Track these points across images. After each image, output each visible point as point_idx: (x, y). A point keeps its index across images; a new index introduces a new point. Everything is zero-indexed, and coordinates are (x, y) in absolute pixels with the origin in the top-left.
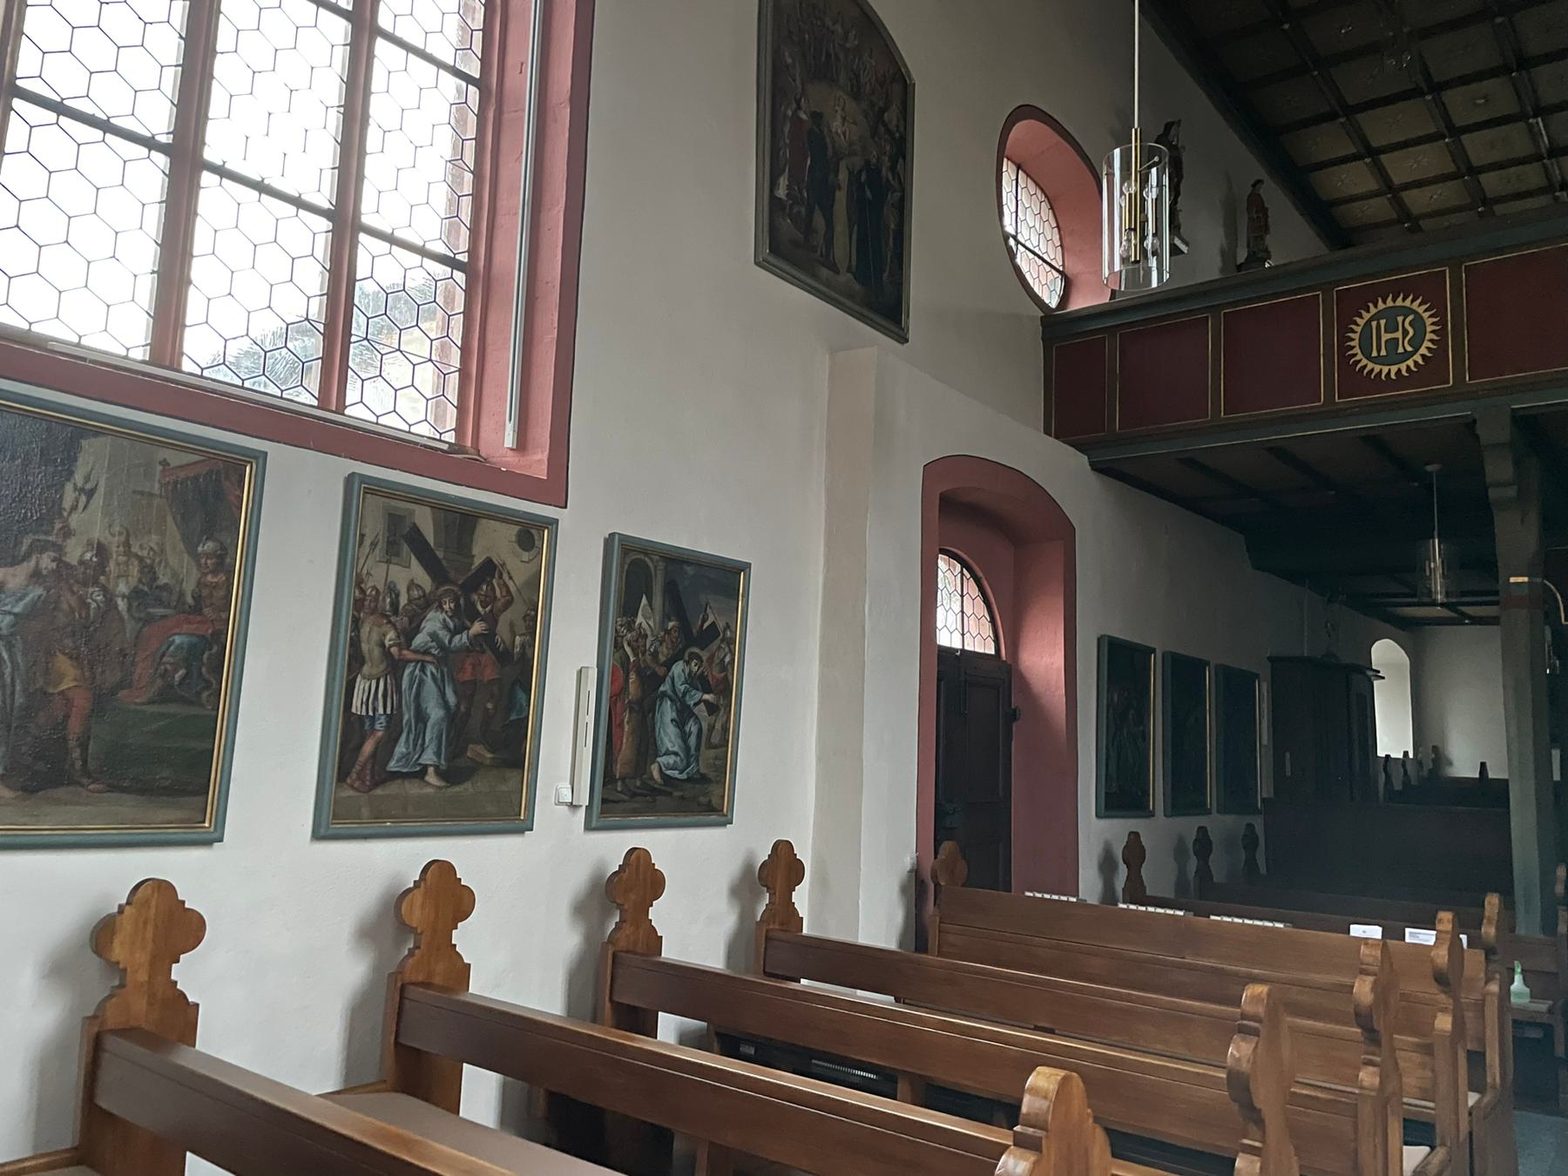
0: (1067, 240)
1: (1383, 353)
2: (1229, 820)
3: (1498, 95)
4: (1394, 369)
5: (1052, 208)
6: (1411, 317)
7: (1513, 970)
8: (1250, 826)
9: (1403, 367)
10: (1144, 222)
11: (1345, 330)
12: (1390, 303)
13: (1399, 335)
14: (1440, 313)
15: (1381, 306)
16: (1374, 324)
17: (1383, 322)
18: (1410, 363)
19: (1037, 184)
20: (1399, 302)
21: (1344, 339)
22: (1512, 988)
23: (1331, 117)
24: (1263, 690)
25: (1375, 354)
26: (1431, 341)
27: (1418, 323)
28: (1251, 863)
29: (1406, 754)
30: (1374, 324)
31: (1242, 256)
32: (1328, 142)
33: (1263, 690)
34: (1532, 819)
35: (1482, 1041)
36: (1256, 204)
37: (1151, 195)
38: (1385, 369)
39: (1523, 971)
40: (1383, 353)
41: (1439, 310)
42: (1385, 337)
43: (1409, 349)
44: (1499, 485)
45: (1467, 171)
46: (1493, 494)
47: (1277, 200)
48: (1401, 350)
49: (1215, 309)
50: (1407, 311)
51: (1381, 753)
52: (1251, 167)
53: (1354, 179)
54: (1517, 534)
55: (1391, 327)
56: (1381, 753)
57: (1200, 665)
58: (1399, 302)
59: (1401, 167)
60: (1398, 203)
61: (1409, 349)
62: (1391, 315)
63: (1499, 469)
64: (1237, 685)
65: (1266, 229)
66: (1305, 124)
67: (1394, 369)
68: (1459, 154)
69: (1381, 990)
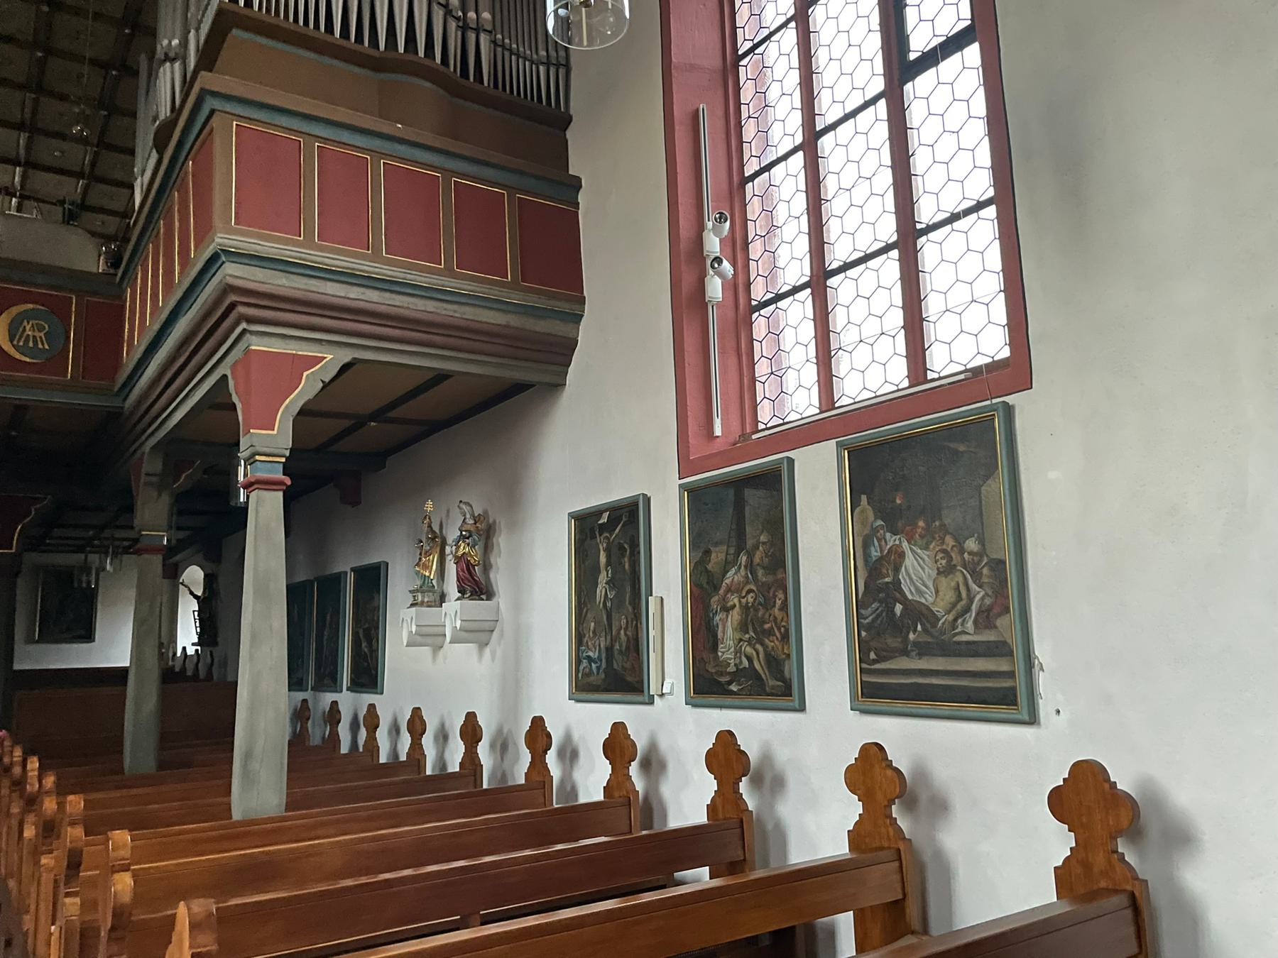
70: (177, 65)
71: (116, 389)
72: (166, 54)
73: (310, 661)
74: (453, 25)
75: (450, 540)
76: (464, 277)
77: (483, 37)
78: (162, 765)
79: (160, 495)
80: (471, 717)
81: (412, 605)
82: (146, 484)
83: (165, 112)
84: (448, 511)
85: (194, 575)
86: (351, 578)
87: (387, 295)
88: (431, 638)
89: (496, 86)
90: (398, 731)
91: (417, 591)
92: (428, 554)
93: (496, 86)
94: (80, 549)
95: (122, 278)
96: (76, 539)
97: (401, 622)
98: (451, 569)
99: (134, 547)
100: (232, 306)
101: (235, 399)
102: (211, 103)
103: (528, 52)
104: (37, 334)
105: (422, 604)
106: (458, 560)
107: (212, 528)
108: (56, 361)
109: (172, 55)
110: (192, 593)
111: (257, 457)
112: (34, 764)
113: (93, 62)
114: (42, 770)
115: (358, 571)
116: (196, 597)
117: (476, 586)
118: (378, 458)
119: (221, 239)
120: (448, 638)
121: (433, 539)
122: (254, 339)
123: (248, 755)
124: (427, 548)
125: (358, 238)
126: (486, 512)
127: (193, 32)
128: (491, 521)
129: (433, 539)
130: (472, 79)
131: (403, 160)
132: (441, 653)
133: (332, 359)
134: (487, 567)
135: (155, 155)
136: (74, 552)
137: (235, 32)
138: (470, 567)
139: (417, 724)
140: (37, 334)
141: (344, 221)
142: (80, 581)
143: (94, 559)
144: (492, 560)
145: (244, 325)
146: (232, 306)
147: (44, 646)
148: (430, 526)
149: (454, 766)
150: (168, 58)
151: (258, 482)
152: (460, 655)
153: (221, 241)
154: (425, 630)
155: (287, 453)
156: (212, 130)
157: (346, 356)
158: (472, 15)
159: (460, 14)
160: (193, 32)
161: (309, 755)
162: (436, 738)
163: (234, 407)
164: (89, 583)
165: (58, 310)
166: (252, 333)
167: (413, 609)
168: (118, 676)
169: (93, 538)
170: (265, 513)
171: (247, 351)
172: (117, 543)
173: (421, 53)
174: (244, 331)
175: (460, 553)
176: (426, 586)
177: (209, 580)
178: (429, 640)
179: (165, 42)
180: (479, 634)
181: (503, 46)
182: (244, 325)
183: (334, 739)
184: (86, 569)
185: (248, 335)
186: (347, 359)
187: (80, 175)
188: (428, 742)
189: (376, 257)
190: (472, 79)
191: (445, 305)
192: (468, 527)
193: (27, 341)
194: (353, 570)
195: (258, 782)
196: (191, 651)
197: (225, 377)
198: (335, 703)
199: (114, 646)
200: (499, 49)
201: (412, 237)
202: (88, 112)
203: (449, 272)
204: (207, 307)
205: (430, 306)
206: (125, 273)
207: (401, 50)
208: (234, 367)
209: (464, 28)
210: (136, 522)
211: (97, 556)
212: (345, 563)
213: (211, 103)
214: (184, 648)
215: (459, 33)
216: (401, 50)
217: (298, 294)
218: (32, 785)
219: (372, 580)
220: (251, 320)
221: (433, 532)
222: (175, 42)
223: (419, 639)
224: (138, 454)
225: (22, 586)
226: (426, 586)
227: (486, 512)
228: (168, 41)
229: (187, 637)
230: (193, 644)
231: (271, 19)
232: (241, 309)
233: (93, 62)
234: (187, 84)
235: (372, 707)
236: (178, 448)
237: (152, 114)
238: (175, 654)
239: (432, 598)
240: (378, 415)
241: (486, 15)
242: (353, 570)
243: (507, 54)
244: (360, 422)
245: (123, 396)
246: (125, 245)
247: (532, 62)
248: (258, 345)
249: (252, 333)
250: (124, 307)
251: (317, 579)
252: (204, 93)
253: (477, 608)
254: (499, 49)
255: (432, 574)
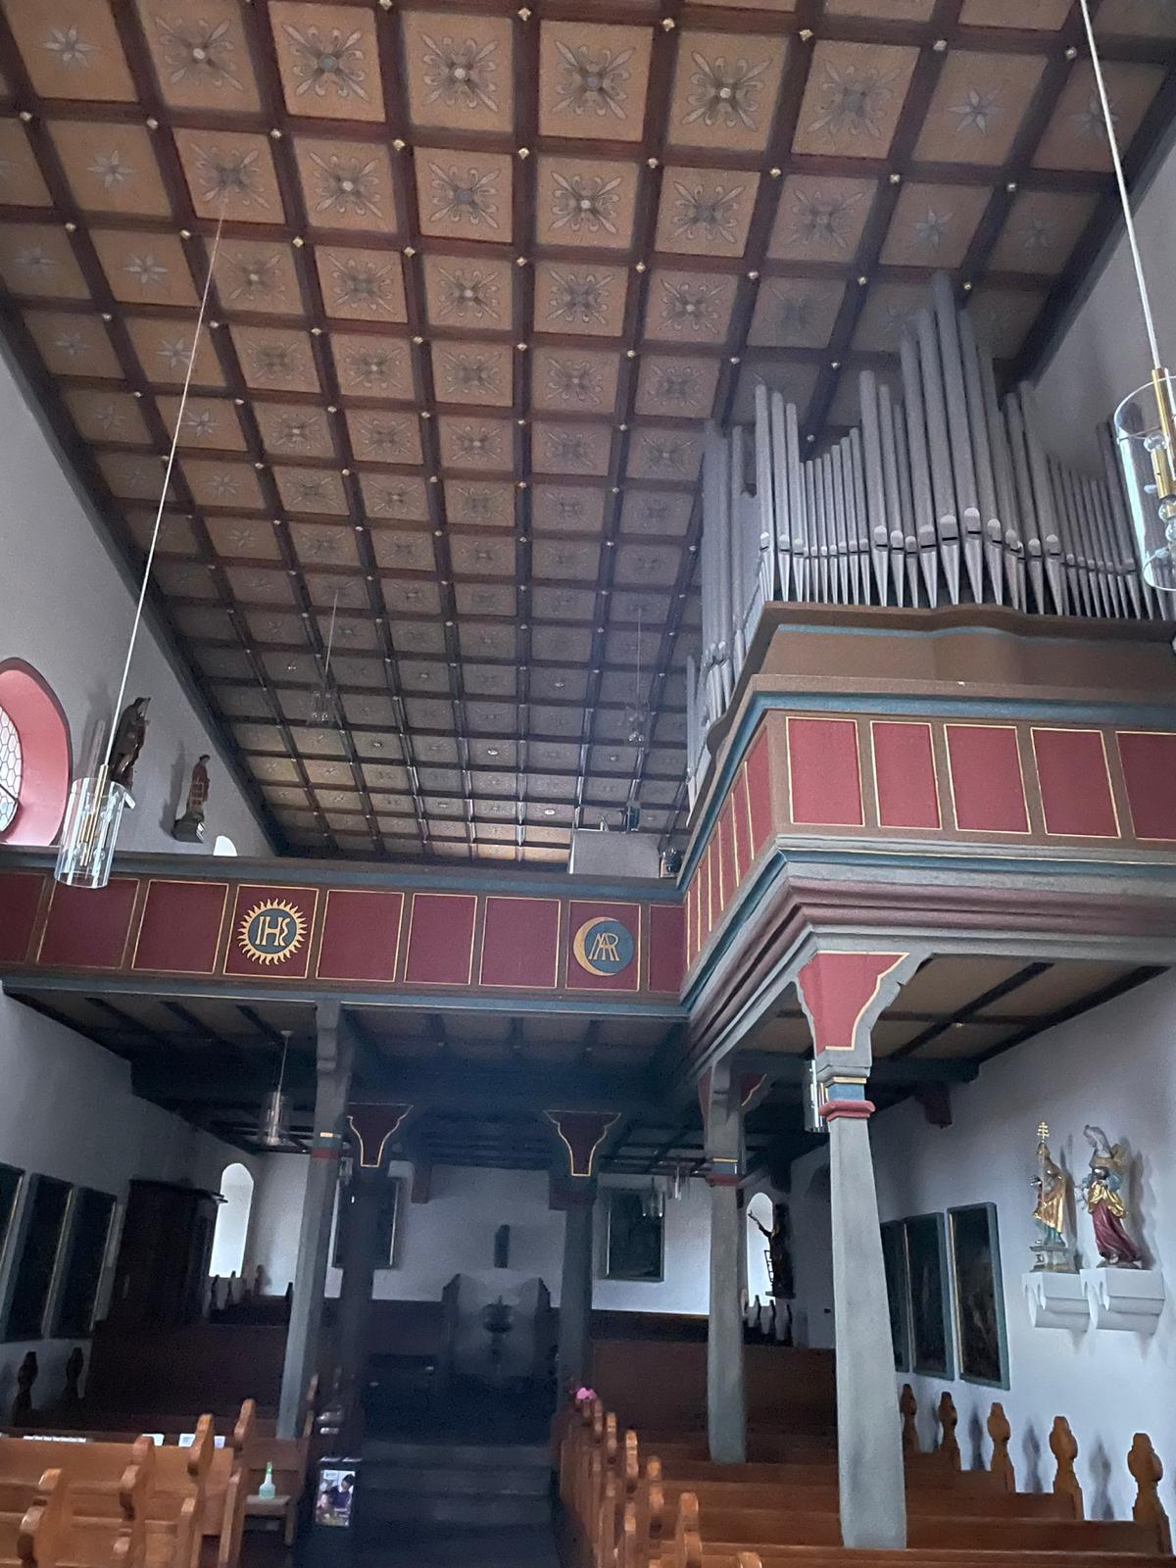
0: (28, 773)
1: (264, 943)
2: (58, 1343)
3: (390, 745)
4: (269, 957)
5: (20, 742)
6: (288, 920)
7: (264, 1471)
8: (78, 1352)
9: (276, 957)
10: (96, 837)
11: (240, 919)
12: (275, 906)
13: (277, 931)
14: (308, 922)
15: (269, 906)
16: (262, 918)
17: (268, 919)
18: (281, 954)
19: (10, 719)
20: (282, 907)
21: (238, 925)
22: (262, 1487)
23: (272, 722)
24: (118, 1212)
25: (258, 942)
26: (298, 941)
27: (292, 925)
28: (72, 1390)
29: (234, 1273)
30: (262, 918)
31: (181, 813)
32: (268, 739)
33: (118, 1212)
34: (303, 1335)
35: (220, 1524)
36: (200, 773)
37: (108, 816)
38: (263, 956)
39: (273, 1472)
40: (264, 943)
41: (307, 916)
42: (268, 931)
43: (282, 944)
44: (585, 784)
45: (362, 788)
46: (320, 1065)
47: (219, 772)
48: (276, 944)
49: (144, 877)
50: (286, 915)
51: (212, 1273)
52: (201, 741)
53: (281, 770)
54: (331, 1098)
55: (273, 925)
56: (212, 1273)
57: (64, 1187)
58: (282, 907)
59: (317, 772)
60: (310, 795)
61: (282, 944)
62: (275, 914)
63: (326, 1048)
64: (95, 1205)
65: (205, 795)
66: (248, 719)
67: (269, 957)
68: (358, 774)
69: (143, 1478)
70: (725, 666)
71: (682, 998)
72: (714, 658)
73: (919, 1343)
74: (1012, 559)
75: (1078, 1181)
76: (1059, 842)
77: (1050, 561)
78: (752, 1454)
79: (728, 1116)
80: (1141, 1440)
81: (1038, 1268)
82: (715, 1102)
83: (716, 714)
84: (1070, 1138)
85: (762, 1205)
86: (949, 1223)
87: (965, 876)
88: (1067, 1316)
89: (1073, 611)
90: (1036, 1448)
91: (1040, 1248)
92: (1050, 1196)
93: (1073, 611)
94: (646, 1171)
95: (682, 882)
96: (641, 1158)
97: (1024, 1295)
98: (1086, 1222)
99: (699, 1167)
100: (796, 909)
101: (805, 1009)
102: (764, 703)
103: (1109, 564)
104: (609, 947)
105: (1050, 1267)
106: (1095, 1209)
107: (785, 1147)
108: (625, 975)
109: (719, 658)
110: (761, 1228)
111: (836, 1079)
112: (632, 1441)
113: (644, 668)
114: (643, 1456)
115: (959, 1214)
116: (766, 1233)
117: (1124, 1248)
118: (968, 1066)
119: (783, 840)
120: (1094, 1318)
121: (1054, 1176)
122: (822, 942)
123: (856, 1461)
124: (1047, 1188)
125: (926, 816)
126: (1124, 1141)
127: (739, 632)
128: (1134, 1154)
129: (1054, 1176)
130: (1042, 612)
131: (971, 719)
132: (1087, 1337)
133: (907, 958)
134: (1137, 1220)
135: (707, 757)
136: (641, 1173)
137: (781, 627)
138: (1112, 1221)
139: (1063, 1443)
140: (609, 947)
141: (909, 802)
142: (648, 1208)
143: (661, 1181)
144: (1143, 1209)
145: (810, 928)
146: (796, 909)
147: (613, 1283)
148: (1048, 1158)
149: (1125, 1513)
150: (716, 661)
151: (838, 1109)
152: (1114, 1347)
153: (782, 841)
154: (1055, 1305)
155: (868, 1073)
156: (766, 728)
157: (924, 951)
158: (1034, 542)
159: (1020, 545)
160: (739, 632)
161: (928, 1468)
162: (1093, 1466)
163: (804, 1016)
164: (656, 1210)
165: (627, 920)
166: (820, 935)
167: (1039, 1274)
168: (693, 1329)
169: (657, 1159)
170: (850, 1147)
171: (816, 957)
172: (684, 1164)
173: (979, 599)
174: (810, 935)
175: (1095, 1200)
176: (1051, 1243)
177: (780, 1212)
178: (1067, 1320)
179: (713, 646)
180: (1138, 1318)
181: (1077, 566)
182: (810, 928)
183: (950, 1448)
184: (653, 1193)
185: (814, 939)
186: (926, 956)
187: (633, 776)
188: (1081, 1467)
189: (948, 834)
190: (1042, 612)
191: (1038, 879)
192: (1103, 1163)
193: (600, 956)
194: (952, 1211)
195: (871, 1504)
196: (765, 1301)
197: (792, 985)
198: (946, 1396)
199: (685, 1288)
200: (1072, 572)
201: (994, 806)
202: (642, 719)
203: (1039, 839)
204: (771, 909)
205: (1020, 882)
206: (684, 878)
207: (955, 600)
208: (802, 973)
209: (1026, 558)
210: (709, 1146)
211: (664, 1179)
212: (940, 1199)
213: (764, 703)
214: (757, 1297)
215: (1021, 567)
216: (955, 600)
217: (863, 888)
218: (633, 1468)
219: (976, 1226)
220: (817, 922)
221: (1054, 1166)
222: (722, 645)
223: (1051, 1317)
224: (704, 1070)
225: (597, 1211)
226: (1051, 1243)
227: (1124, 1141)
228: (714, 643)
229: (760, 1284)
230: (767, 1294)
231: (816, 606)
232: (806, 911)
233: (644, 668)
234: (739, 687)
235: (997, 1409)
236: (744, 1060)
237: (702, 714)
238: (747, 1304)
239: (1064, 1260)
240: (966, 1013)
241: (1052, 538)
242: (952, 1211)
243: (1082, 572)
244: (941, 1024)
245: (688, 1006)
246: (678, 840)
247: (1116, 574)
248: (826, 947)
249: (820, 935)
250: (683, 911)
251: (905, 1220)
252: (756, 695)
253: (1129, 1278)
254: (1072, 572)
255: (1059, 1224)
